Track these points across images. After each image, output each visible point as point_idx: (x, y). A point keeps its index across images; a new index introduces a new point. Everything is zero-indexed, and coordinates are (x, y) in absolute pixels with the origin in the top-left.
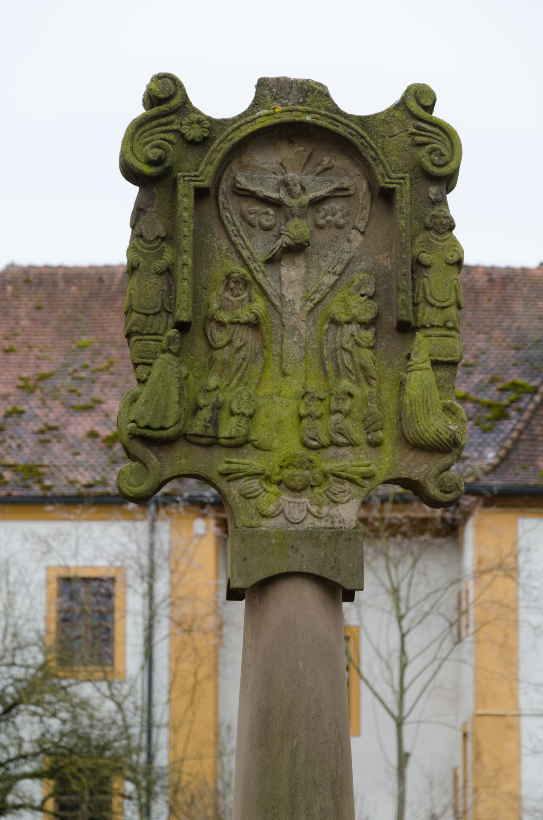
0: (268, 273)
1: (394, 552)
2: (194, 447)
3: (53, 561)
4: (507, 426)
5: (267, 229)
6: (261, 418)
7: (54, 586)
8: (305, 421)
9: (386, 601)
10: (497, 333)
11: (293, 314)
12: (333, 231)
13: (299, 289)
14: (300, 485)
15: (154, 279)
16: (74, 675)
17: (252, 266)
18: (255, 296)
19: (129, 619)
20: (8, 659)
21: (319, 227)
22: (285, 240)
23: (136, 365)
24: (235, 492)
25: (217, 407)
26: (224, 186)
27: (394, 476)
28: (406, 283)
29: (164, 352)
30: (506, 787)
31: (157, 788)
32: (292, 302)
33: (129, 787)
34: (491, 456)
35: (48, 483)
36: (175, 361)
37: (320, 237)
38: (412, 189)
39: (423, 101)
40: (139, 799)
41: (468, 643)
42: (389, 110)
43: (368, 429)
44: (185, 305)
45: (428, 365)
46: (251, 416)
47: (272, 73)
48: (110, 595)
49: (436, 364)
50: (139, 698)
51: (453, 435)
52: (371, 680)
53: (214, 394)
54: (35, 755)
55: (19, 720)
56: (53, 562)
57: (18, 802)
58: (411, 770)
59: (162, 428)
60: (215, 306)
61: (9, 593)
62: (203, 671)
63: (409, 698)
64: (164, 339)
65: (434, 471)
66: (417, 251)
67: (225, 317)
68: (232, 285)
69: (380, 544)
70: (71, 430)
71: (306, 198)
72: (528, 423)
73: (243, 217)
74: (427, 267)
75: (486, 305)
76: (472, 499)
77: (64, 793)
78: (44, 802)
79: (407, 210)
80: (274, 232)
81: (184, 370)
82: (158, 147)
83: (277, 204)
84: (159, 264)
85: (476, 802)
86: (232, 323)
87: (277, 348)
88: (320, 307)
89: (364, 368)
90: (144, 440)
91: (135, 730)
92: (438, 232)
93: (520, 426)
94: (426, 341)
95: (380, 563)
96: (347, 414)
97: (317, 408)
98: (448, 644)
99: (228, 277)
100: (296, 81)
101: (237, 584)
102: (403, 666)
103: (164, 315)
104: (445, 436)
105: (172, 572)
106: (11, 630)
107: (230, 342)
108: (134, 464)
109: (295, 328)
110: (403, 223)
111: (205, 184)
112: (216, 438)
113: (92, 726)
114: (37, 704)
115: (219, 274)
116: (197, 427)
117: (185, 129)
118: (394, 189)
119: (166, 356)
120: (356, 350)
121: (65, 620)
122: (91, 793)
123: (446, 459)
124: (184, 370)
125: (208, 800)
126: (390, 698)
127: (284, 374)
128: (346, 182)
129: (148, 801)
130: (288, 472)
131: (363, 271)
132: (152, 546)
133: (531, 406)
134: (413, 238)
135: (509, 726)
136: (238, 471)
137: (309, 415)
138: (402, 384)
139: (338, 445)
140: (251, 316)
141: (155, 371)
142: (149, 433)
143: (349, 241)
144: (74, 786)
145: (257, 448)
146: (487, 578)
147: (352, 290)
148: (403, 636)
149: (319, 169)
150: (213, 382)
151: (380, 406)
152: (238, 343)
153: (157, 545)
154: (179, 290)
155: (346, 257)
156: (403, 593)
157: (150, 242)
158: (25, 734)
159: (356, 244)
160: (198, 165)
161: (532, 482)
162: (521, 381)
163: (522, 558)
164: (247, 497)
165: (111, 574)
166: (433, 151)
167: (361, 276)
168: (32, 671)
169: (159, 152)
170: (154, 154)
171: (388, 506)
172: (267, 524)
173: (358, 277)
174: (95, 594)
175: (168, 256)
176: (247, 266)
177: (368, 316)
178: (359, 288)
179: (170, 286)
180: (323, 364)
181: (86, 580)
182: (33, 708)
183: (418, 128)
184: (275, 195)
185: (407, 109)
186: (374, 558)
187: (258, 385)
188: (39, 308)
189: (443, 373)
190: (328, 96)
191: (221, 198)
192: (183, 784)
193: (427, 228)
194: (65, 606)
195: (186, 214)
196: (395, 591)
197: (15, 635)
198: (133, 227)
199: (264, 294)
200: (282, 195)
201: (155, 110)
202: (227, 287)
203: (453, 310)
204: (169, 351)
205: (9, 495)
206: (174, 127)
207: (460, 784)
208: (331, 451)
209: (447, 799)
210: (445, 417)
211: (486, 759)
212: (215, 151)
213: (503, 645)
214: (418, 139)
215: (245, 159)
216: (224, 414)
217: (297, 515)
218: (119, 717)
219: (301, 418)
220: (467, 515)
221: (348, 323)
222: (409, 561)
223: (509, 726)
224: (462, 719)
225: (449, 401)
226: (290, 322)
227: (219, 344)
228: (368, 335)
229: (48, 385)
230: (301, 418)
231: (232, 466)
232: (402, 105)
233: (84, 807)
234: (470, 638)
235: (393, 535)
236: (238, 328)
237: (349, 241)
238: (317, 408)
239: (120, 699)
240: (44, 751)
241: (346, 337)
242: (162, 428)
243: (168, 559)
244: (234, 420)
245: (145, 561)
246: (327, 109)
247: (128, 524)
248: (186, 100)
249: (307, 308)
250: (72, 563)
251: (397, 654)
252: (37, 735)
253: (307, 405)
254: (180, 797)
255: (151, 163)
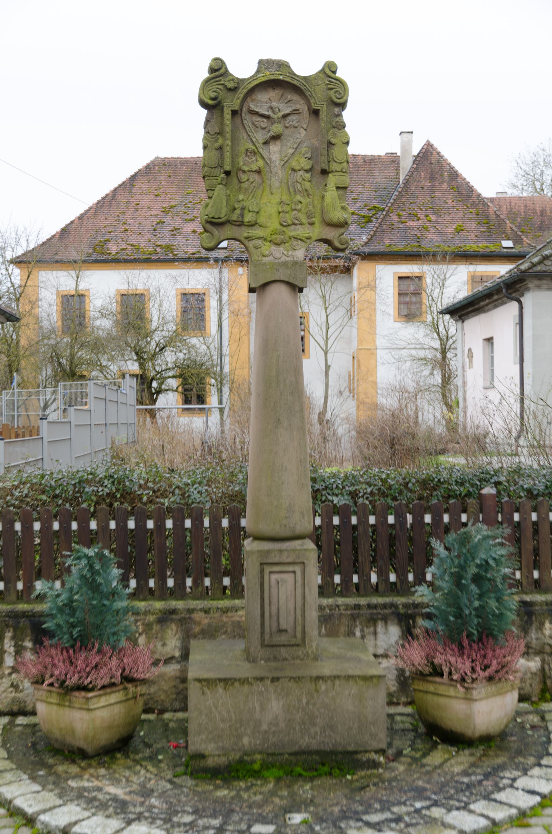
0: (264, 148)
1: (323, 280)
2: (233, 227)
3: (178, 286)
4: (371, 225)
5: (264, 129)
6: (262, 213)
7: (179, 297)
8: (281, 214)
9: (320, 301)
10: (367, 185)
11: (275, 167)
12: (293, 129)
13: (278, 155)
14: (279, 242)
15: (214, 152)
16: (189, 334)
17: (257, 145)
18: (259, 159)
19: (212, 311)
20: (161, 328)
21: (287, 127)
22: (271, 134)
23: (207, 190)
24: (251, 246)
25: (243, 209)
26: (244, 109)
27: (320, 238)
28: (325, 152)
29: (219, 184)
30: (370, 379)
31: (225, 382)
32: (275, 161)
33: (213, 381)
34: (364, 238)
35: (175, 253)
36: (224, 188)
37: (287, 132)
38: (327, 110)
39: (332, 69)
40: (217, 386)
41: (355, 319)
42: (317, 74)
43: (309, 217)
44: (228, 163)
45: (334, 188)
46: (258, 212)
47: (265, 57)
48: (203, 301)
49: (338, 188)
50: (216, 343)
51: (345, 219)
52: (314, 335)
53: (242, 203)
54: (173, 368)
55: (166, 354)
56: (179, 287)
57: (167, 388)
58: (331, 372)
59: (219, 218)
60: (241, 163)
61: (160, 300)
62: (243, 332)
63: (330, 342)
64: (219, 179)
65: (337, 235)
66: (329, 137)
67: (246, 168)
68: (249, 154)
69: (318, 277)
70: (185, 229)
71: (280, 114)
72: (380, 224)
73: (253, 124)
74: (333, 145)
75: (363, 172)
76: (357, 257)
77: (186, 384)
78: (177, 388)
79: (325, 119)
80: (267, 130)
81: (228, 192)
82: (215, 91)
83: (268, 117)
84: (217, 145)
85: (358, 385)
86: (249, 171)
87: (269, 182)
88: (287, 164)
89: (306, 190)
90: (211, 223)
91: (215, 357)
92: (338, 129)
93: (377, 225)
94: (333, 178)
95: (318, 285)
96: (299, 211)
97: (286, 208)
98: (346, 319)
99: (247, 150)
100: (275, 60)
101: (253, 286)
102: (328, 329)
103: (219, 168)
104: (342, 220)
105: (229, 290)
106: (162, 316)
107: (248, 180)
108: (208, 234)
109: (276, 173)
110: (323, 125)
111: (236, 108)
112: (243, 222)
113: (197, 356)
114: (173, 347)
115: (242, 149)
116: (234, 217)
117: (227, 83)
118: (319, 110)
119: (221, 186)
120: (303, 183)
121: (184, 311)
122: (197, 384)
123: (342, 230)
124: (228, 192)
125: (246, 385)
126: (322, 343)
127: (272, 194)
128: (298, 107)
129: (221, 387)
130: (274, 237)
131: (306, 147)
132: (220, 279)
133: (382, 216)
134: (328, 132)
135: (372, 354)
136: (252, 236)
137: (283, 211)
138: (323, 197)
139: (295, 224)
140: (257, 168)
141: (216, 193)
142: (214, 220)
143: (299, 133)
144: (190, 381)
145: (260, 226)
146: (363, 291)
147: (301, 155)
148: (327, 316)
149: (286, 101)
150: (241, 197)
151: (314, 207)
152: (251, 180)
153: (223, 279)
154: (226, 156)
155: (298, 141)
156: (327, 298)
157: (212, 135)
158: (169, 359)
159: (303, 135)
160: (233, 100)
161: (382, 249)
162: (377, 206)
163: (377, 282)
164: (256, 248)
165: (203, 292)
166: (336, 92)
167: (305, 149)
168: (171, 333)
169: (215, 94)
170: (213, 95)
171: (321, 261)
172: (265, 259)
173: (303, 150)
174: (197, 300)
175: (220, 141)
176: (254, 145)
177: (308, 167)
178: (304, 155)
179: (221, 155)
180: (289, 189)
181: (193, 294)
182: (172, 349)
183: (330, 81)
184: (267, 113)
185: (325, 73)
186: (315, 283)
187: (261, 198)
188: (170, 177)
189: (341, 192)
190: (289, 67)
191: (243, 115)
192: (235, 379)
193: (334, 127)
194: (184, 305)
195: (228, 122)
196: (324, 297)
197: (163, 318)
198: (205, 128)
199: (263, 158)
200: (269, 113)
201: (213, 75)
202: (246, 155)
203: (345, 164)
204: (222, 184)
205: (159, 258)
206: (222, 82)
207: (352, 378)
208: (293, 227)
209: (346, 384)
210: (342, 211)
211: (362, 367)
212: (240, 93)
213: (369, 319)
214: (330, 86)
215: (254, 97)
216: (246, 212)
217: (278, 255)
218: (208, 352)
219: (279, 213)
220: (354, 264)
221: (300, 170)
222: (330, 284)
223: (372, 354)
224: (352, 351)
225: (343, 205)
226: (274, 170)
227: (244, 180)
228: (308, 175)
229: (174, 210)
230: (279, 213)
231: (250, 235)
232: (323, 71)
233: (194, 390)
234: (356, 317)
235: (323, 273)
236: (251, 173)
237: (299, 133)
238: (286, 208)
239: (208, 345)
240: (176, 366)
241: (299, 177)
242: (219, 218)
243: (227, 285)
244: (250, 214)
245: (218, 286)
246: (289, 73)
247: (210, 270)
248: (227, 70)
249: (282, 164)
250: (187, 287)
251: (325, 324)
252: (174, 360)
253: (282, 207)
254: (234, 385)
255: (212, 99)
